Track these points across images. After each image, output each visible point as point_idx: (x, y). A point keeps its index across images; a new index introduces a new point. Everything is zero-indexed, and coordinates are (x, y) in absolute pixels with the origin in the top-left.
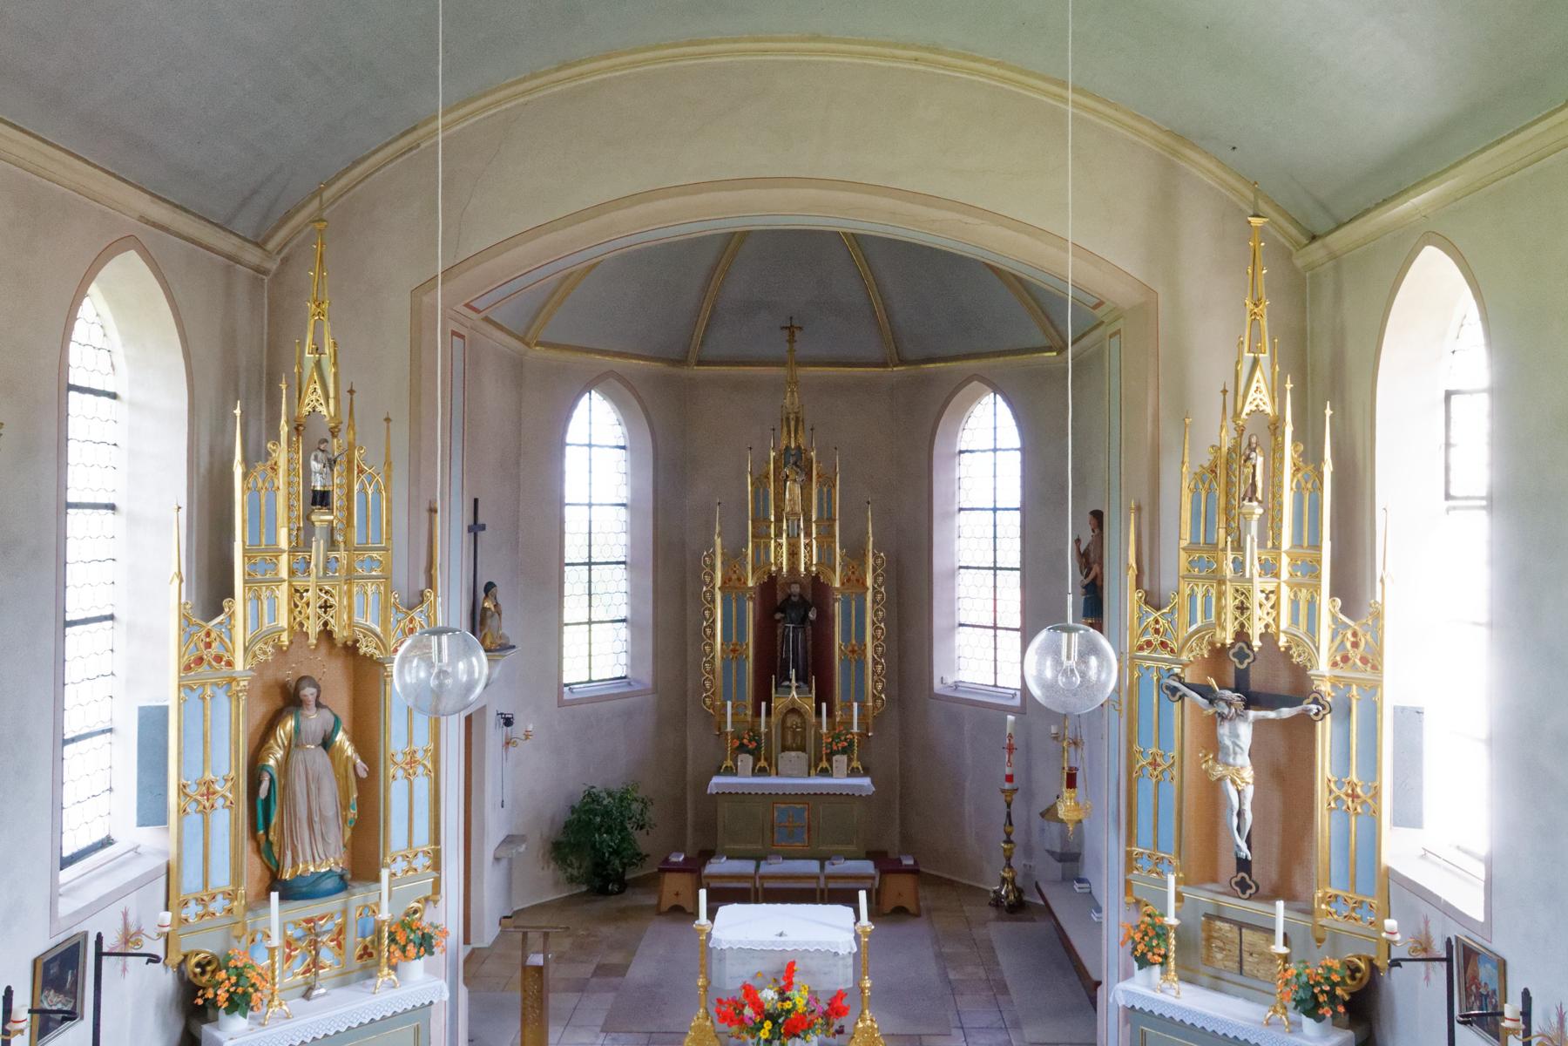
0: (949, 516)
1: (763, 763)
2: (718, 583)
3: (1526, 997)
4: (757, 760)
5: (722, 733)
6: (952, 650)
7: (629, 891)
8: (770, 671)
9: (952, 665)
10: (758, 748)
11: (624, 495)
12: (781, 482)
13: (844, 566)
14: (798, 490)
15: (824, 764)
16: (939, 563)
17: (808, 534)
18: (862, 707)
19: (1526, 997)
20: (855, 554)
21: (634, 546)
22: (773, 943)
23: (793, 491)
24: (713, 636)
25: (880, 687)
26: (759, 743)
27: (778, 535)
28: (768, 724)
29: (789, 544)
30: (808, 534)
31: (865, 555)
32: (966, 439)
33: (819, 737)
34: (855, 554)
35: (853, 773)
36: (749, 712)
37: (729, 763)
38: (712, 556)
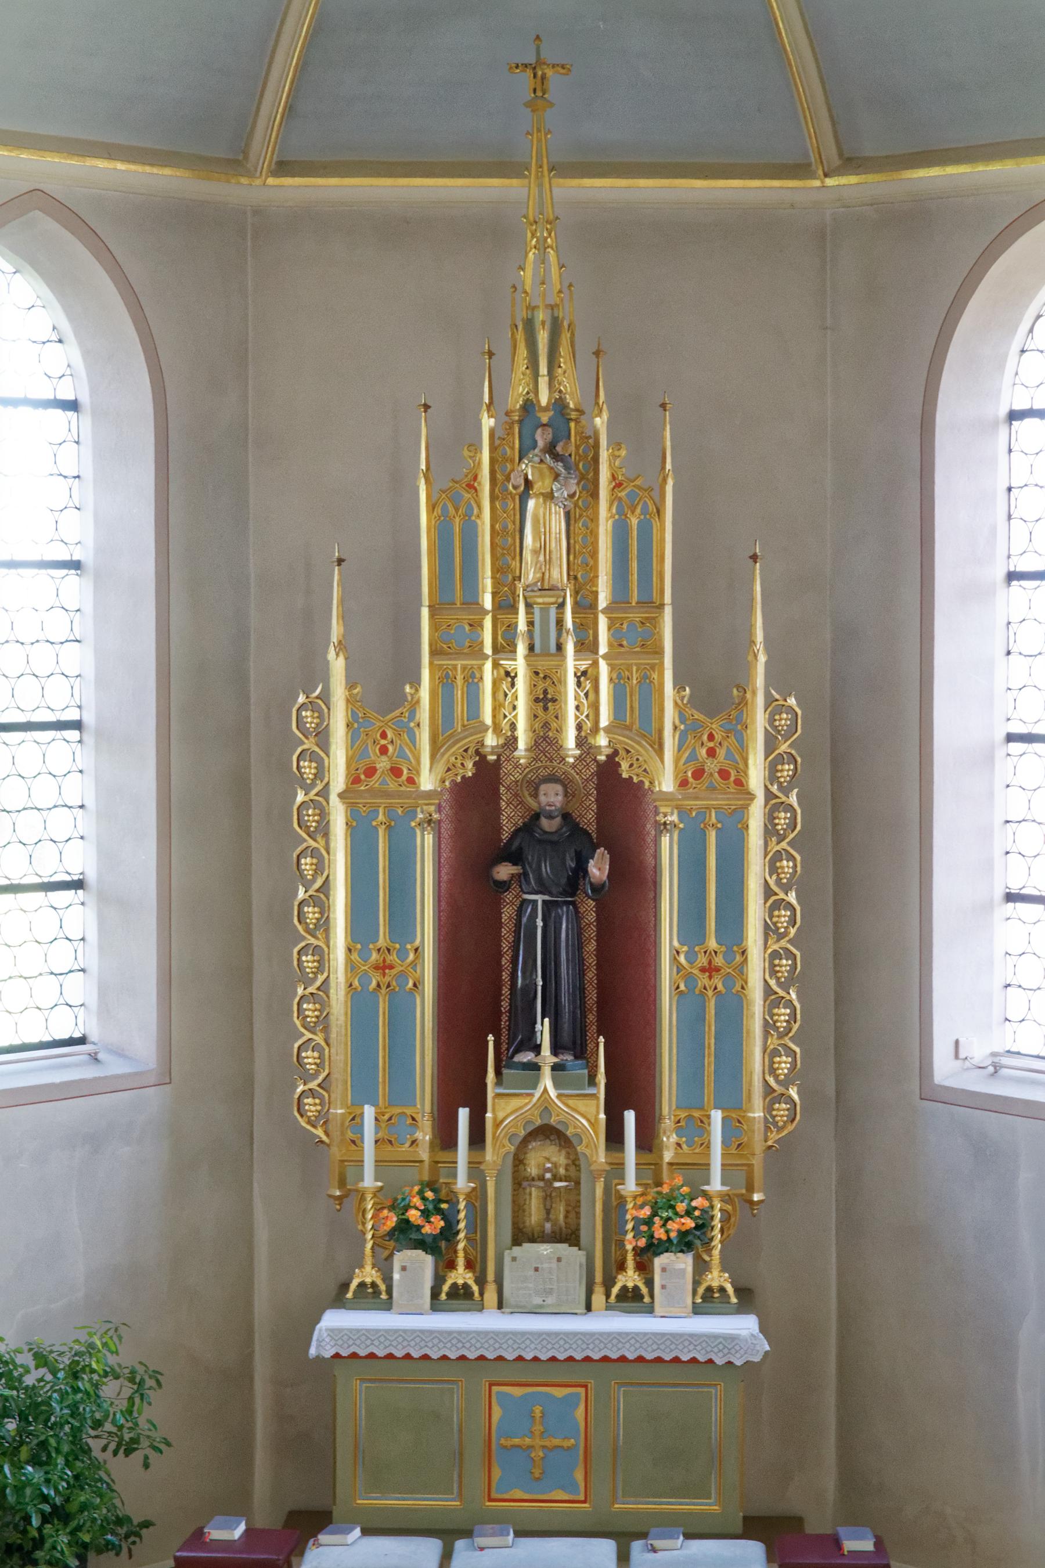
1: (461, 1275)
2: (338, 780)
8: (482, 1022)
10: (449, 1233)
13: (688, 731)
14: (557, 523)
15: (630, 1278)
17: (587, 645)
18: (734, 1126)
20: (715, 698)
23: (545, 523)
24: (324, 925)
27: (504, 647)
28: (475, 1170)
30: (587, 645)
33: (614, 1205)
34: (715, 698)
35: (709, 1301)
36: (425, 1135)
37: (368, 1274)
38: (321, 705)
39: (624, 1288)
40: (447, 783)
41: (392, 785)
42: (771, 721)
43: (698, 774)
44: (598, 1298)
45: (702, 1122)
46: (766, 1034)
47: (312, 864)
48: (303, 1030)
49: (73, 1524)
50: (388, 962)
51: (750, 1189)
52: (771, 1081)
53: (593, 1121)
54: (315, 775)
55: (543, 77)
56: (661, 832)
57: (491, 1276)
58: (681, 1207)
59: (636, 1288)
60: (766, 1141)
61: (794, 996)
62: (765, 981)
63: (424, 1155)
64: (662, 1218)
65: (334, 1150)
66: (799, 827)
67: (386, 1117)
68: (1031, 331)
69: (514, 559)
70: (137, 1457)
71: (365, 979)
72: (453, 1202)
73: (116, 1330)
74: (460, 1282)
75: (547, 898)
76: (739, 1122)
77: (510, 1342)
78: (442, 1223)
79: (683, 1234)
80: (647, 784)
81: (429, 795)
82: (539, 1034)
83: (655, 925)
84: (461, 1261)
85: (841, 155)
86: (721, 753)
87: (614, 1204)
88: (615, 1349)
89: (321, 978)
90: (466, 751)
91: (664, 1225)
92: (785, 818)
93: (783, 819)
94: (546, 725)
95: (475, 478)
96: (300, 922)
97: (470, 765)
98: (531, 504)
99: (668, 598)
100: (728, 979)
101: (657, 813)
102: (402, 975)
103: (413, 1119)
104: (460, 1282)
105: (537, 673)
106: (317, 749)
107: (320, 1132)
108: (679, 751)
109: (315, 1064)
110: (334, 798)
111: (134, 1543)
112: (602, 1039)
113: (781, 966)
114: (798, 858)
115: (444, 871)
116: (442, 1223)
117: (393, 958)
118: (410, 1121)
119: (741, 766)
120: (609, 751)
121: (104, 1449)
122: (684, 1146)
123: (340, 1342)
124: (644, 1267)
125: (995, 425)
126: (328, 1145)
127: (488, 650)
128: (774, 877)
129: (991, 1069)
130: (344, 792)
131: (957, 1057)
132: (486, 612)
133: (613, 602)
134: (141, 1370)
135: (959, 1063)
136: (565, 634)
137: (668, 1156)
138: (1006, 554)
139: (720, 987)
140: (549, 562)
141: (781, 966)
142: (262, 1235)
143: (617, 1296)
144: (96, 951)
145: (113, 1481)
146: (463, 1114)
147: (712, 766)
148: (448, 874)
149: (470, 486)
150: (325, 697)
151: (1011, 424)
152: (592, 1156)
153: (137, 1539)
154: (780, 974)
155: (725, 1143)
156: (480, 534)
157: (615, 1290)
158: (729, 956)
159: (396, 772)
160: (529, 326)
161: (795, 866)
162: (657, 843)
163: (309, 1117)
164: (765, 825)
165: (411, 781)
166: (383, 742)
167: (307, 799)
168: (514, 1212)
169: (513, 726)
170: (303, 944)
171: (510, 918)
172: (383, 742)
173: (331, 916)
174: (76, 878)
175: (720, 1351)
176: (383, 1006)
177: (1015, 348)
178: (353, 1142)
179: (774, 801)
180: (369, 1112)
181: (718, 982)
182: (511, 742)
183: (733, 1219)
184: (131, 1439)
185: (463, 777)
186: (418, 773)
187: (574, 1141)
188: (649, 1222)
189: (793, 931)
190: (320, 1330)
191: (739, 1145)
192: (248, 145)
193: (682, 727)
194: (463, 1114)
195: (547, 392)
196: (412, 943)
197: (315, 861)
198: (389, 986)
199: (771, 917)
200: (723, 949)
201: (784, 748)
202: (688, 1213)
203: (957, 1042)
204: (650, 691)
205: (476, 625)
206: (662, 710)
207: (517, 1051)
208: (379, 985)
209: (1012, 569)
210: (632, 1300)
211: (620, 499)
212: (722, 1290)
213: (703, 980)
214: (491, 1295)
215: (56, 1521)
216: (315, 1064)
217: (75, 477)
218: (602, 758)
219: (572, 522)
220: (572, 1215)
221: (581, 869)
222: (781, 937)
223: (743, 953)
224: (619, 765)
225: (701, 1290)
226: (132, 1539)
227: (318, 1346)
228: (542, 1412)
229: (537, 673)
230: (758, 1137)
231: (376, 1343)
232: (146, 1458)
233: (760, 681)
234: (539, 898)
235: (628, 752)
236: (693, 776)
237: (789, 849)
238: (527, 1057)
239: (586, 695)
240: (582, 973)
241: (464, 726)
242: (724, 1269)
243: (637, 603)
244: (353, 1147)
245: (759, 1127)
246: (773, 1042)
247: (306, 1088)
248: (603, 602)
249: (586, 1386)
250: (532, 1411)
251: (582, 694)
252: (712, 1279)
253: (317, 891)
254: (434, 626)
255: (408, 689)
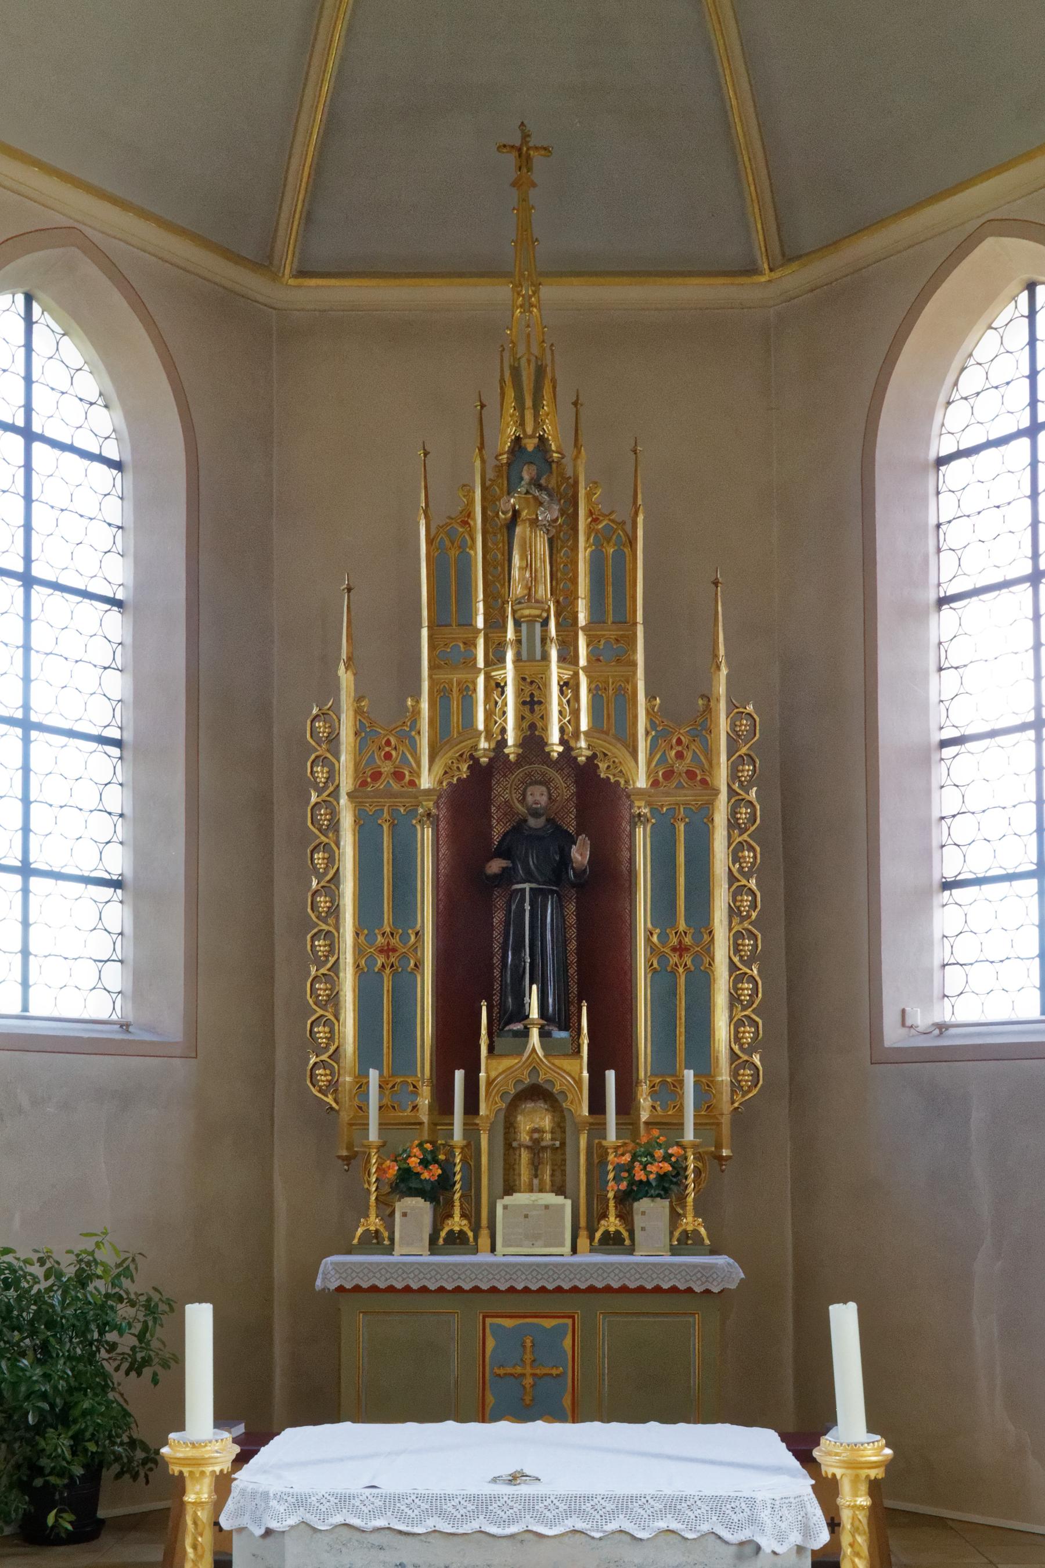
0: (917, 615)
1: (457, 1223)
2: (346, 782)
3: (495, 1480)
4: (442, 1215)
5: (354, 1158)
6: (926, 944)
7: (106, 1538)
8: (474, 993)
9: (927, 984)
10: (445, 1182)
11: (115, 575)
12: (503, 531)
13: (659, 735)
14: (541, 546)
15: (612, 1223)
16: (893, 728)
17: (568, 657)
18: (705, 1087)
19: (495, 1480)
20: (683, 722)
21: (141, 698)
22: (482, 1504)
23: (530, 558)
24: (335, 911)
25: (748, 1036)
26: (447, 1167)
27: (495, 659)
28: (471, 1131)
29: (522, 679)
30: (568, 657)
31: (708, 710)
32: (955, 425)
33: (597, 1158)
34: (683, 722)
35: (685, 1243)
36: (425, 1100)
37: (374, 1222)
38: (330, 715)
39: (606, 1233)
40: (444, 784)
41: (395, 786)
42: (733, 726)
43: (669, 775)
44: (583, 1242)
45: (674, 1086)
46: (731, 1007)
47: (324, 859)
48: (314, 1007)
49: (75, 1428)
50: (392, 944)
51: (719, 1146)
52: (736, 1048)
53: (577, 1078)
54: (327, 779)
55: (529, 158)
56: (636, 824)
57: (484, 1222)
58: (659, 1153)
59: (618, 1233)
60: (733, 1103)
61: (755, 972)
62: (730, 958)
63: (425, 1119)
64: (641, 1162)
65: (342, 1114)
66: (758, 821)
67: (390, 1086)
68: (956, 384)
69: (503, 585)
70: (147, 1371)
71: (371, 960)
72: (451, 1153)
73: (133, 1260)
74: (457, 1228)
75: (534, 885)
76: (708, 1086)
77: (503, 1273)
78: (440, 1172)
79: (662, 1177)
80: (623, 782)
81: (428, 792)
82: (527, 1006)
83: (630, 911)
84: (457, 1211)
85: (783, 255)
86: (689, 756)
87: (596, 1161)
88: (600, 1279)
89: (332, 960)
90: (461, 755)
91: (645, 1169)
92: (746, 813)
93: (744, 813)
94: (533, 726)
95: (469, 516)
96: (312, 909)
97: (464, 767)
98: (518, 530)
99: (640, 618)
100: (697, 958)
101: (631, 807)
102: (404, 957)
103: (415, 1087)
104: (457, 1228)
105: (524, 679)
106: (328, 755)
107: (329, 1099)
108: (651, 754)
109: (326, 1038)
110: (344, 800)
111: (151, 1469)
112: (584, 1004)
113: (744, 945)
114: (758, 849)
115: (442, 865)
116: (440, 1172)
117: (395, 942)
118: (411, 1088)
119: (706, 766)
120: (589, 753)
121: (117, 1369)
122: (659, 1108)
123: (344, 1275)
124: (626, 1217)
125: (925, 467)
126: (337, 1112)
127: (481, 664)
128: (737, 866)
129: (937, 1032)
130: (355, 790)
131: (903, 1024)
132: (479, 631)
133: (590, 623)
134: (156, 1297)
135: (904, 1031)
136: (548, 641)
137: (644, 1116)
138: (936, 582)
139: (689, 963)
140: (535, 579)
141: (744, 945)
142: (281, 1204)
143: (600, 1240)
144: (132, 943)
145: (125, 1401)
146: (459, 1075)
147: (680, 767)
148: (444, 868)
149: (465, 523)
150: (336, 708)
151: (938, 470)
152: (576, 1111)
153: (152, 1465)
154: (743, 953)
155: (697, 1107)
156: (473, 563)
157: (598, 1235)
158: (697, 936)
159: (398, 776)
160: (516, 372)
161: (755, 857)
162: (632, 836)
163: (320, 1087)
164: (728, 820)
165: (412, 783)
166: (387, 749)
167: (319, 800)
168: (505, 1169)
169: (503, 731)
170: (316, 930)
171: (500, 922)
172: (387, 749)
173: (341, 903)
174: (115, 878)
175: (698, 1279)
176: (387, 984)
177: (942, 399)
178: (360, 1108)
179: (737, 798)
180: (374, 1075)
181: (688, 959)
182: (502, 743)
183: (703, 1175)
184: (143, 1358)
185: (459, 779)
186: (419, 776)
187: (560, 1098)
188: (629, 1168)
189: (754, 915)
190: (326, 1264)
191: (708, 1107)
192: (272, 249)
193: (653, 733)
194: (459, 1075)
195: (532, 423)
196: (413, 928)
197: (326, 855)
198: (392, 966)
199: (735, 900)
200: (692, 931)
201: (744, 750)
202: (667, 1158)
203: (903, 1011)
204: (626, 699)
205: (471, 644)
206: (636, 717)
207: (507, 1023)
208: (383, 966)
209: (942, 595)
210: (612, 1242)
211: (597, 532)
212: (696, 1232)
213: (674, 958)
214: (484, 1240)
215: (60, 1427)
216: (326, 1038)
217: (119, 527)
218: (582, 759)
219: (555, 551)
220: (558, 1173)
221: (566, 859)
222: (743, 919)
223: (710, 932)
224: (597, 766)
225: (677, 1234)
226: (150, 1465)
227: (324, 1279)
228: (532, 1342)
229: (524, 679)
230: (726, 1096)
231: (378, 1275)
232: (155, 1374)
233: (722, 690)
234: (527, 886)
235: (605, 755)
236: (664, 776)
237: (749, 840)
238: (518, 1026)
239: (568, 702)
240: (565, 942)
241: (458, 732)
242: (697, 1215)
243: (613, 623)
244: (362, 1113)
245: (726, 1090)
246: (739, 1015)
247: (318, 1060)
248: (582, 619)
249: (573, 1318)
250: (524, 1342)
251: (565, 701)
252: (687, 1224)
253: (329, 882)
254: (432, 647)
255: (409, 702)
